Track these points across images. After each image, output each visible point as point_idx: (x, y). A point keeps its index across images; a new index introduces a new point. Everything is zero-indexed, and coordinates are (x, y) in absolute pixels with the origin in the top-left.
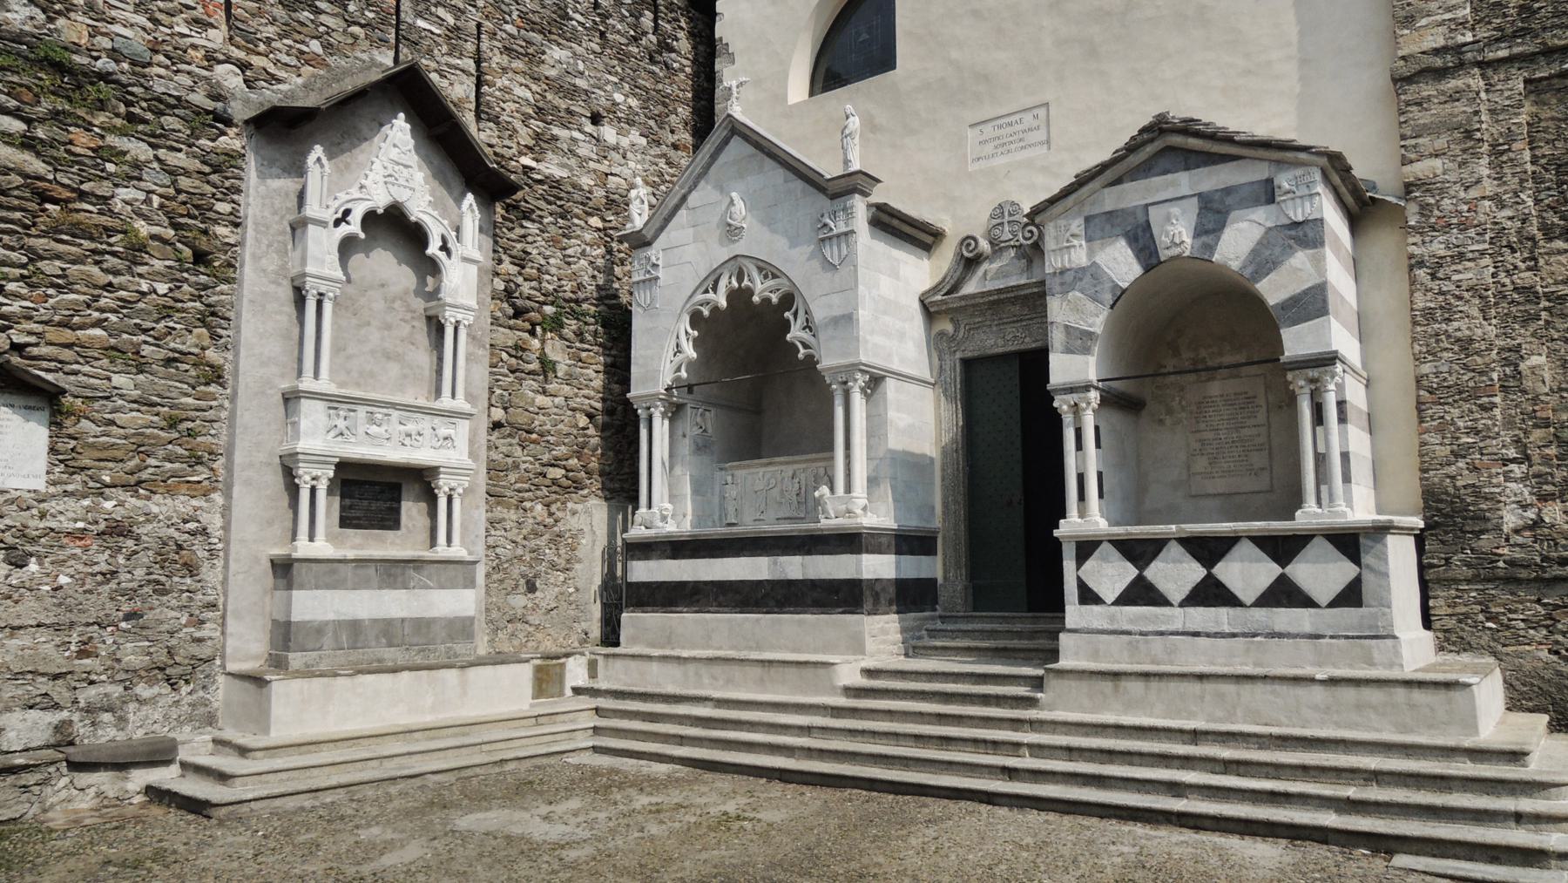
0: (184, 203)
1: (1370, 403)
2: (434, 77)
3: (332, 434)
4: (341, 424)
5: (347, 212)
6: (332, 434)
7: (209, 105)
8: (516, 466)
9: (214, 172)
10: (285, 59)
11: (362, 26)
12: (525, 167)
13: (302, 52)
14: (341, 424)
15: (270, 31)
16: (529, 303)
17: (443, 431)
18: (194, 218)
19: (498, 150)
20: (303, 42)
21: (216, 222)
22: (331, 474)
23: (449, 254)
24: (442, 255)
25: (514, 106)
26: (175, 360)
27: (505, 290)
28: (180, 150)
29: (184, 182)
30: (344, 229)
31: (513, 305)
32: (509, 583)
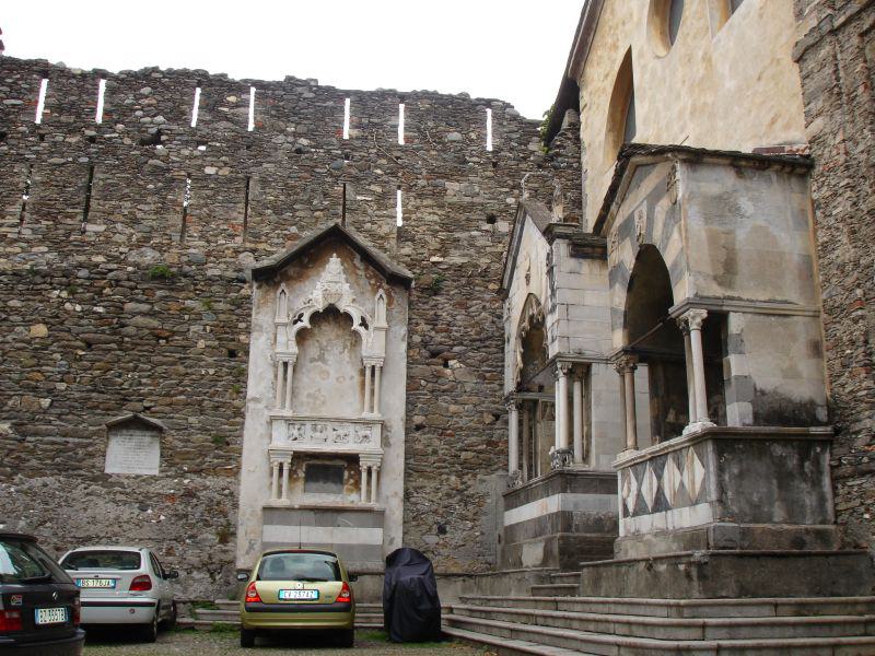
5: (301, 315)
7: (234, 275)
8: (435, 452)
10: (276, 241)
12: (433, 263)
13: (285, 235)
14: (296, 433)
15: (266, 230)
17: (363, 432)
23: (366, 327)
24: (362, 330)
26: (218, 407)
30: (299, 325)
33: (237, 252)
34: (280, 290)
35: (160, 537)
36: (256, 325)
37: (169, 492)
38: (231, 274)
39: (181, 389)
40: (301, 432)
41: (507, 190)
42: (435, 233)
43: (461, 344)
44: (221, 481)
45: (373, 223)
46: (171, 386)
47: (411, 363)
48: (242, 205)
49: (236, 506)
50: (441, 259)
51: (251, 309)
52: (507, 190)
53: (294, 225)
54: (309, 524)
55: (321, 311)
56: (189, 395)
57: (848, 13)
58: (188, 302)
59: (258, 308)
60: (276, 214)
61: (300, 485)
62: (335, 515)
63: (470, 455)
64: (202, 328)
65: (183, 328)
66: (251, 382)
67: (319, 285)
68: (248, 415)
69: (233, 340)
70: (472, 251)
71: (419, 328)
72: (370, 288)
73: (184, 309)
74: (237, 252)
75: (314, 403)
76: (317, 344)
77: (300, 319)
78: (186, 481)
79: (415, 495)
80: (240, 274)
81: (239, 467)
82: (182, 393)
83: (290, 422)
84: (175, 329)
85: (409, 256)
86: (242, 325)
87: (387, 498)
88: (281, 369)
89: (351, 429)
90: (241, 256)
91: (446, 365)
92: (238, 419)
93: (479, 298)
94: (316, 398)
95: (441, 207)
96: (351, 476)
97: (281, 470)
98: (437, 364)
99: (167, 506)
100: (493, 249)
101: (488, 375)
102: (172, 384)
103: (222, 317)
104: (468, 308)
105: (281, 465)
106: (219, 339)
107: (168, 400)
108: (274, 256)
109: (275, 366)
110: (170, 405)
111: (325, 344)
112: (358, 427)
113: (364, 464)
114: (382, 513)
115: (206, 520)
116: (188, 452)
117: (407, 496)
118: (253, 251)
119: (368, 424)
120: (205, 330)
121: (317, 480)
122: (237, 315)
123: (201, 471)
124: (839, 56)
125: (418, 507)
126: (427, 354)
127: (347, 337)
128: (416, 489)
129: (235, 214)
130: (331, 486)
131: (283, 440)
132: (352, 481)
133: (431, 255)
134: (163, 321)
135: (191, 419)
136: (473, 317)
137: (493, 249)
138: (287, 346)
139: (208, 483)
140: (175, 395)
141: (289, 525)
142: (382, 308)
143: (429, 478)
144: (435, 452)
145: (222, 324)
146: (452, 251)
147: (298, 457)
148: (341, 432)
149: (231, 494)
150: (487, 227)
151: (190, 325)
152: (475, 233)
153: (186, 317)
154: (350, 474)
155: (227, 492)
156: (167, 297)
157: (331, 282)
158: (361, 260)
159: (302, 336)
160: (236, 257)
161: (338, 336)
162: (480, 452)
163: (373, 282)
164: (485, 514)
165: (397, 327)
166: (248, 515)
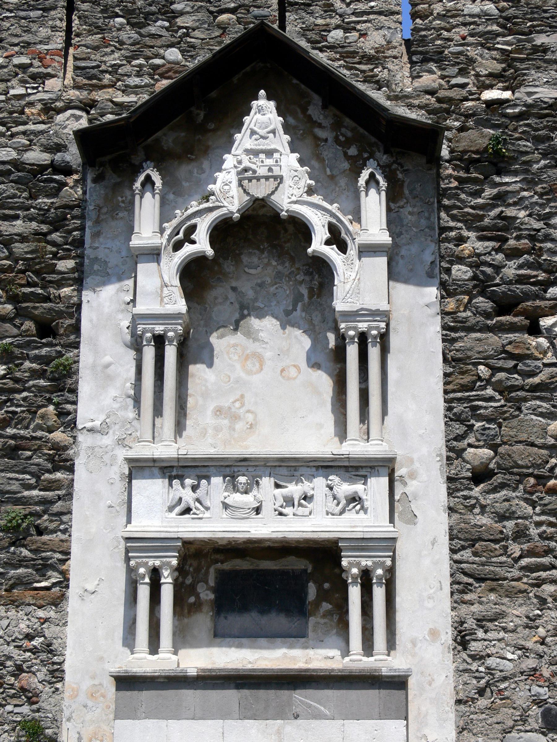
0: (23, 272)
1: (90, 2)
2: (227, 41)
3: (178, 509)
4: (188, 496)
5: (193, 229)
6: (178, 509)
7: (44, 158)
8: (520, 535)
9: (56, 230)
10: (134, 81)
11: (233, 11)
12: (490, 104)
13: (155, 68)
14: (188, 496)
15: (114, 59)
16: (519, 288)
17: (345, 489)
18: (35, 285)
19: (442, 94)
20: (157, 56)
21: (59, 284)
22: (174, 562)
23: (343, 248)
24: (332, 253)
25: (464, 31)
26: (17, 448)
27: (474, 278)
28: (16, 217)
29: (19, 248)
30: (188, 249)
31: (492, 297)
32: (507, 715)
33: (49, 110)
34: (142, 178)
36: (96, 260)
38: (36, 156)
40: (200, 492)
42: (487, 40)
45: (347, 28)
47: (452, 328)
48: (60, 13)
49: (57, 674)
50: (507, 95)
53: (172, 45)
54: (224, 715)
59: (97, 222)
60: (133, 25)
61: (203, 621)
62: (284, 694)
66: (85, 388)
67: (229, 160)
68: (79, 464)
69: (47, 299)
71: (467, 248)
72: (346, 165)
74: (49, 110)
75: (232, 428)
76: (232, 296)
77: (188, 239)
79: (480, 634)
80: (58, 157)
81: (64, 583)
83: (173, 470)
85: (432, 92)
87: (414, 643)
88: (149, 353)
89: (318, 485)
90: (60, 118)
92: (59, 475)
94: (235, 418)
96: (323, 596)
98: (512, 328)
103: (19, 248)
105: (155, 573)
109: (136, 345)
111: (251, 294)
112: (334, 479)
114: (399, 683)
117: (462, 640)
119: (357, 468)
121: (244, 609)
125: (491, 662)
127: (300, 277)
128: (481, 622)
129: (44, 32)
130: (278, 621)
131: (156, 511)
132: (326, 606)
138: (159, 291)
141: (135, 717)
142: (374, 204)
143: (512, 594)
145: (20, 265)
147: (196, 555)
148: (294, 489)
149: (48, 648)
154: (320, 589)
157: (263, 156)
158: (325, 107)
159: (194, 276)
160: (50, 120)
161: (279, 276)
163: (353, 151)
165: (414, 249)
166: (82, 698)
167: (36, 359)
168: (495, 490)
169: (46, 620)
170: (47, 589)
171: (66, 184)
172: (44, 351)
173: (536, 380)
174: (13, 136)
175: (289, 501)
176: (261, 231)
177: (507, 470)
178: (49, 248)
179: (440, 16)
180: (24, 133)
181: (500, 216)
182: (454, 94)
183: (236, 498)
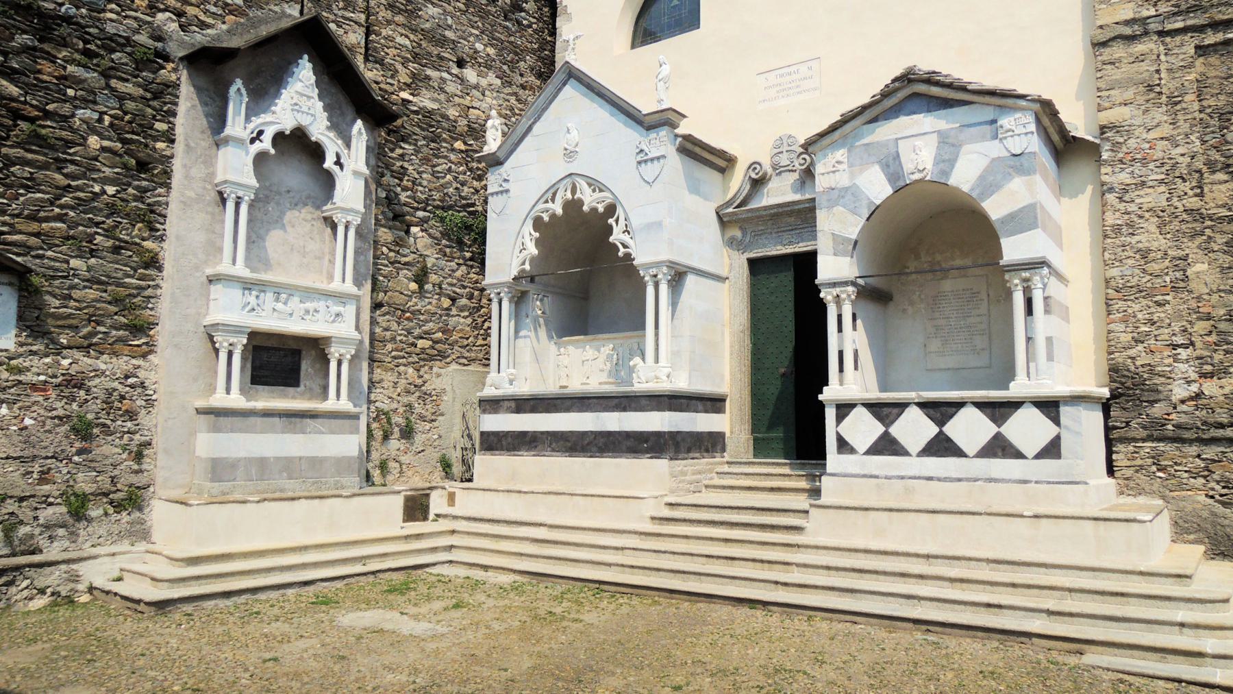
4: (252, 300)
5: (261, 133)
8: (393, 339)
10: (213, 9)
12: (403, 100)
17: (336, 309)
19: (382, 86)
21: (156, 139)
22: (245, 341)
24: (336, 168)
25: (395, 52)
26: (121, 248)
28: (127, 80)
29: (130, 105)
30: (258, 146)
35: (26, 453)
37: (35, 378)
39: (57, 210)
40: (260, 302)
41: (477, 32)
43: (425, 210)
44: (122, 364)
46: (41, 204)
50: (411, 98)
51: (176, 104)
52: (477, 32)
55: (288, 132)
56: (73, 225)
57: (1190, 22)
58: (71, 68)
63: (428, 343)
64: (96, 116)
65: (66, 109)
70: (442, 97)
73: (65, 78)
78: (65, 362)
80: (160, 45)
82: (60, 218)
84: (50, 107)
86: (161, 126)
89: (321, 305)
90: (160, 16)
91: (407, 232)
93: (445, 157)
95: (414, 31)
97: (230, 354)
99: (35, 403)
100: (461, 101)
101: (448, 250)
102: (42, 200)
103: (130, 105)
104: (434, 166)
106: (124, 142)
107: (34, 227)
108: (209, 31)
110: (37, 235)
112: (330, 303)
113: (334, 352)
115: (104, 425)
116: (69, 316)
118: (180, 14)
120: (100, 120)
122: (154, 109)
123: (89, 346)
124: (1163, 57)
126: (391, 215)
133: (401, 89)
134: (27, 88)
135: (74, 263)
136: (438, 178)
137: (461, 101)
139: (103, 367)
140: (47, 220)
144: (393, 339)
146: (424, 91)
149: (142, 385)
150: (455, 70)
151: (76, 107)
152: (445, 75)
153: (70, 92)
155: (131, 381)
156: (34, 49)
157: (300, 100)
162: (436, 342)
164: (442, 415)
167: (137, 188)
168: (384, 315)
169: (139, 367)
170: (138, 346)
171: (164, 68)
172: (144, 183)
173: (406, 259)
174: (126, 17)
175: (307, 312)
176: (297, 144)
177: (389, 305)
178: (150, 111)
179: (385, 38)
180: (135, 18)
181: (402, 167)
182: (387, 87)
183: (280, 306)
